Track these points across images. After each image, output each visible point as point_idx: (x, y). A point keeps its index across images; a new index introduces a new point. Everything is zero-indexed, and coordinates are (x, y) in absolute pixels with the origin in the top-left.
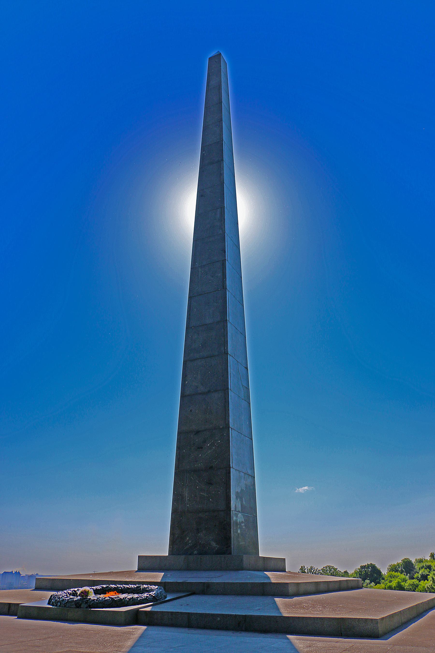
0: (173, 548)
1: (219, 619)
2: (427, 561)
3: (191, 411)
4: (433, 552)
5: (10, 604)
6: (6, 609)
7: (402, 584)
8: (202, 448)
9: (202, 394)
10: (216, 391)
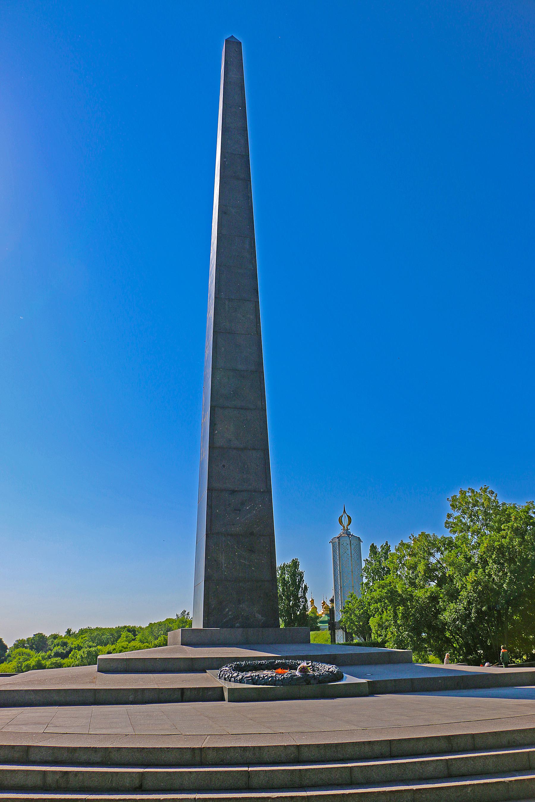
0: (208, 620)
1: (440, 681)
2: (61, 637)
3: (224, 466)
4: (70, 627)
5: (183, 689)
6: (178, 695)
7: (43, 662)
8: (240, 510)
9: (236, 449)
10: (254, 449)
